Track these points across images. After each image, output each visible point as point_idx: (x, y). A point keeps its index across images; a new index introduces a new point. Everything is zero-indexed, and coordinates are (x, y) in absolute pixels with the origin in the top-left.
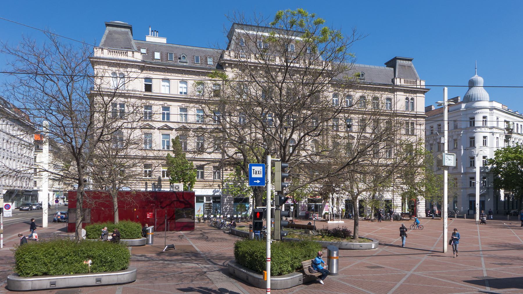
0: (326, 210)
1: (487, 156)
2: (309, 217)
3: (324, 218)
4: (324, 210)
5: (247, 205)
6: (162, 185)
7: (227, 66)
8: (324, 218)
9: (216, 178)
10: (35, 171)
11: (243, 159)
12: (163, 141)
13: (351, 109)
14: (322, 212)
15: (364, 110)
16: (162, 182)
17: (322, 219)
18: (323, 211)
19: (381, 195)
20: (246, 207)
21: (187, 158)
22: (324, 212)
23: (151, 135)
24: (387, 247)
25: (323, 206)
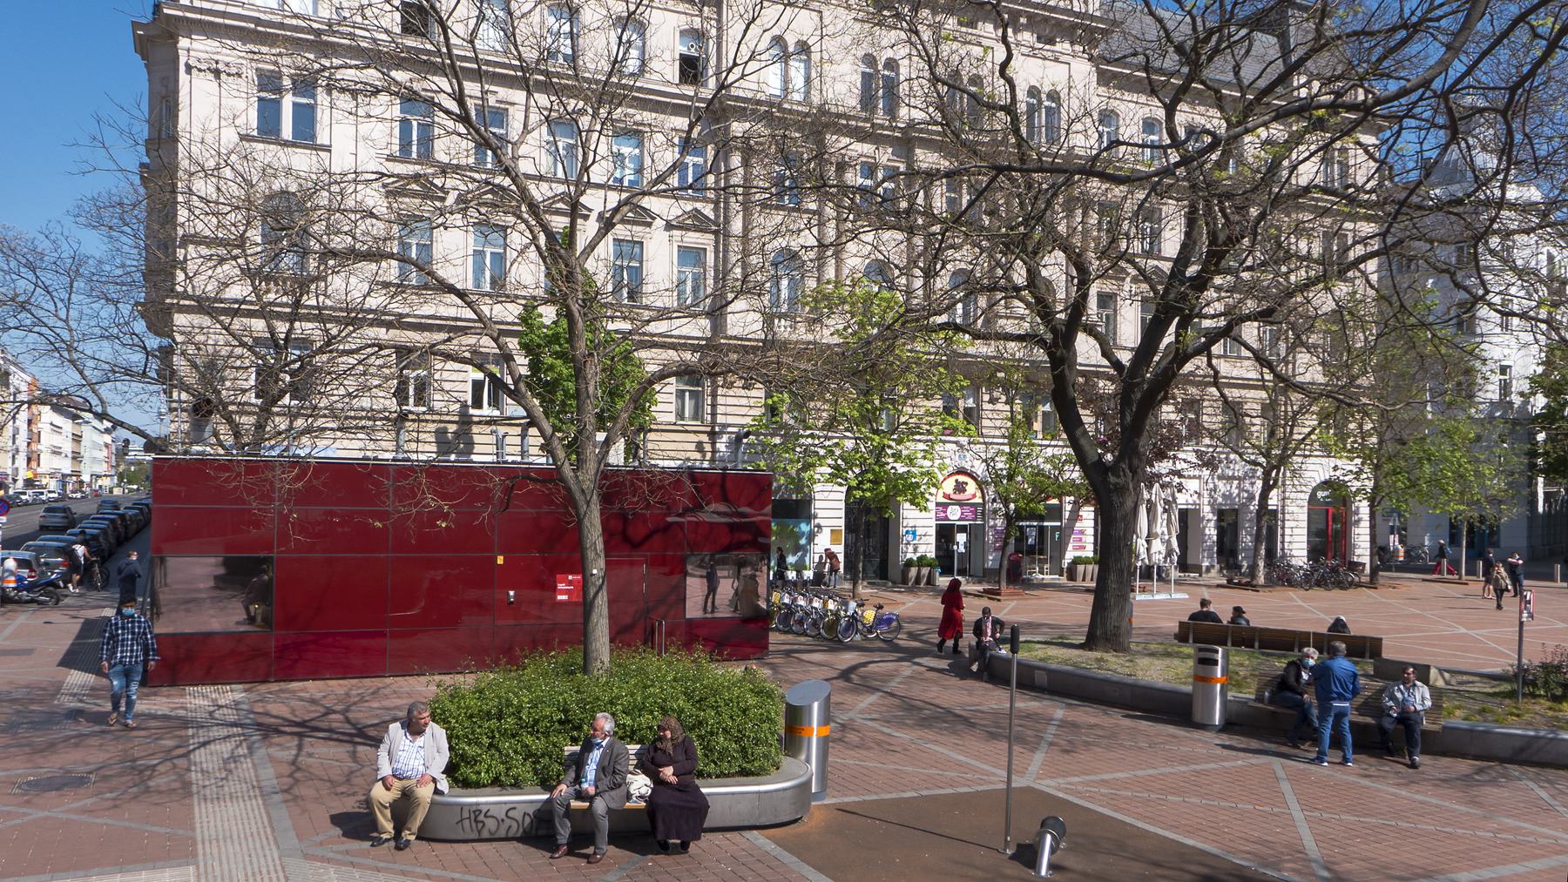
0: (1075, 549)
1: (1510, 367)
2: (1021, 575)
3: (1072, 576)
4: (1070, 547)
5: (804, 527)
6: (477, 439)
7: (1022, 25)
8: (1072, 576)
9: (687, 415)
10: (422, 387)
11: (1046, 362)
12: (478, 254)
13: (638, 84)
14: (1062, 556)
15: (632, 83)
16: (475, 429)
17: (1063, 580)
18: (1065, 550)
19: (1247, 491)
20: (801, 535)
21: (1081, 365)
22: (1070, 555)
23: (637, 250)
24: (332, 743)
25: (1067, 531)
